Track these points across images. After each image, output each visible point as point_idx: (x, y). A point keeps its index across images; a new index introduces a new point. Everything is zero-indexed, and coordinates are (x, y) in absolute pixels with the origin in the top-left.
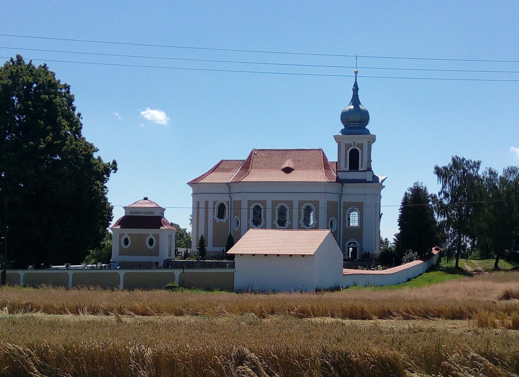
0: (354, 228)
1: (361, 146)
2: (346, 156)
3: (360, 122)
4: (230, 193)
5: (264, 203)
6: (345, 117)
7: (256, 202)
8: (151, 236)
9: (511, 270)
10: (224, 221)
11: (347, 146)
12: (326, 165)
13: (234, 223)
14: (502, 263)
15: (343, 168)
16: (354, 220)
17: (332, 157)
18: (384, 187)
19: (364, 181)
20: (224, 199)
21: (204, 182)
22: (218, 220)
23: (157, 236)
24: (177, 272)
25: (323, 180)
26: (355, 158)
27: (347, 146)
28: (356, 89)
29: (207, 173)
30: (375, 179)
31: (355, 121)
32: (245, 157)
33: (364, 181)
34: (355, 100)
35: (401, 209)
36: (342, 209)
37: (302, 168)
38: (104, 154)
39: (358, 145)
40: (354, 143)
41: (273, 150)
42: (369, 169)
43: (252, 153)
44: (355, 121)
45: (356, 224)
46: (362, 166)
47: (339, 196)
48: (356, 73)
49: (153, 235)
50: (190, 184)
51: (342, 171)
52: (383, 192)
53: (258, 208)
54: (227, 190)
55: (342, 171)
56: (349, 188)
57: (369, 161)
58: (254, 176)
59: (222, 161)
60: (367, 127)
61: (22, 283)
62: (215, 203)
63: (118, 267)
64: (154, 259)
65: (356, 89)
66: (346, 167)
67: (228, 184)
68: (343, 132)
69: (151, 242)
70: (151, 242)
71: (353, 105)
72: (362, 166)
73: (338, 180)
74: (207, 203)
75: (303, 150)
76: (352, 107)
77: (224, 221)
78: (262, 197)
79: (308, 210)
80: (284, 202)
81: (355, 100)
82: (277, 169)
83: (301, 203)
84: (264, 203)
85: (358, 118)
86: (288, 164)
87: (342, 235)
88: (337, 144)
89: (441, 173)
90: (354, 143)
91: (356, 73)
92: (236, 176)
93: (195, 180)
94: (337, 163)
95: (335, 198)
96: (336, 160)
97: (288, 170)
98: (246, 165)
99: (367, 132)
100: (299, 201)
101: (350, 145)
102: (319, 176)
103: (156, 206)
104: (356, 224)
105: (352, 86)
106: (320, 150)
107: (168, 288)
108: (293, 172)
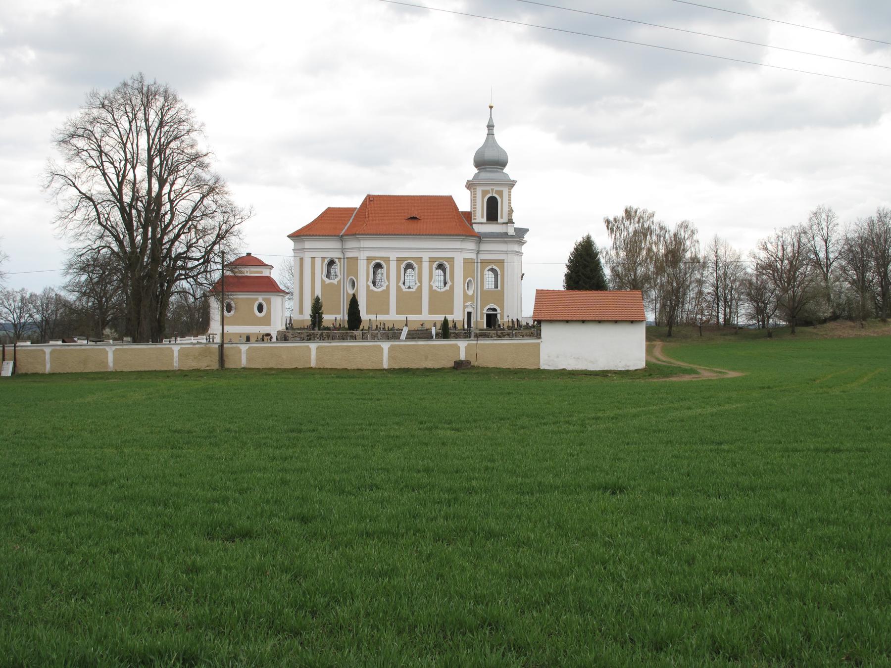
22: (327, 281)
40: (492, 190)
84: (387, 260)
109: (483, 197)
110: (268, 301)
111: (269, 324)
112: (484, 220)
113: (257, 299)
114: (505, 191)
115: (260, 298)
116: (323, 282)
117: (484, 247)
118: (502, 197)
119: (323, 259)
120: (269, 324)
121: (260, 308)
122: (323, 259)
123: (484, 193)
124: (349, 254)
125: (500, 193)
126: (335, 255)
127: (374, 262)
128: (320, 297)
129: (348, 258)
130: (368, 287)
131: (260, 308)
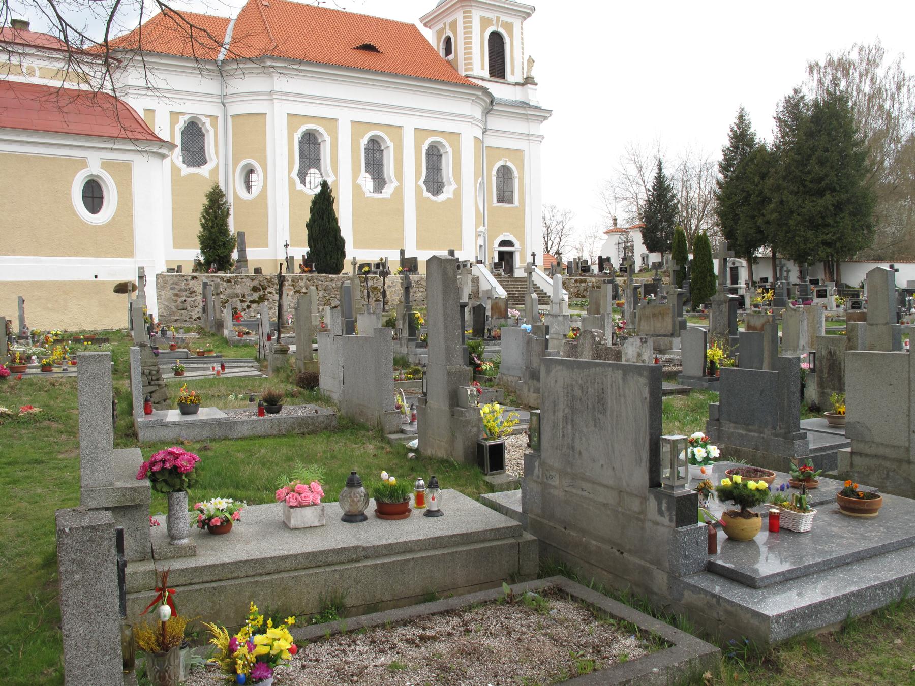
22: (186, 170)
40: (498, 19)
46: (513, 73)
66: (483, 68)
72: (513, 73)
84: (331, 123)
109: (482, 31)
110: (123, 172)
111: (128, 251)
112: (486, 73)
113: (83, 163)
114: (516, 22)
115: (95, 162)
117: (495, 122)
118: (511, 36)
119: (175, 115)
120: (128, 251)
121: (93, 195)
122: (175, 115)
123: (485, 22)
124: (238, 108)
125: (509, 27)
126: (201, 109)
127: (304, 128)
128: (222, 186)
129: (233, 116)
130: (292, 183)
131: (93, 195)
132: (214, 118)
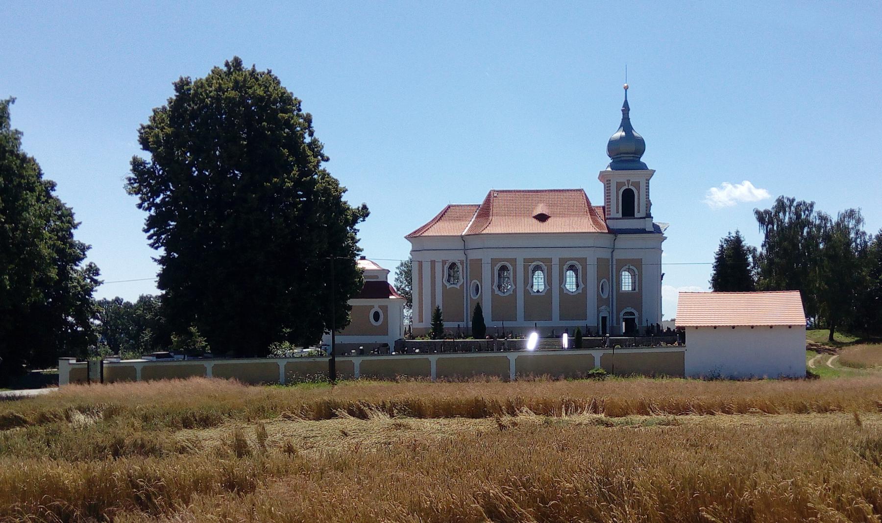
0: (627, 293)
1: (637, 185)
2: (617, 199)
3: (635, 153)
4: (465, 250)
5: (513, 261)
6: (614, 148)
7: (572, 259)
8: (376, 309)
9: (853, 343)
10: (458, 287)
11: (619, 185)
12: (592, 211)
13: (472, 290)
14: (838, 337)
15: (613, 214)
16: (627, 283)
17: (598, 199)
18: (666, 238)
19: (643, 231)
20: (456, 257)
21: (430, 234)
22: (449, 286)
23: (385, 309)
24: (433, 358)
25: (592, 230)
26: (629, 203)
27: (619, 185)
28: (626, 109)
29: (430, 223)
30: (657, 230)
31: (627, 153)
32: (481, 201)
33: (643, 231)
34: (626, 124)
35: (716, 266)
36: (614, 270)
37: (562, 215)
38: (352, 200)
39: (633, 184)
40: (628, 181)
41: (519, 191)
42: (649, 216)
43: (489, 195)
44: (627, 153)
45: (542, 288)
47: (611, 250)
48: (626, 88)
49: (380, 307)
50: (409, 237)
51: (613, 219)
52: (664, 245)
53: (504, 268)
54: (460, 245)
55: (613, 219)
56: (624, 241)
57: (649, 205)
58: (498, 226)
59: (449, 207)
60: (642, 160)
61: (512, 377)
62: (444, 262)
63: (417, 351)
64: (380, 339)
65: (626, 109)
66: (618, 212)
67: (462, 236)
68: (611, 165)
69: (376, 316)
70: (376, 316)
71: (624, 130)
73: (611, 231)
74: (433, 263)
75: (537, 191)
76: (624, 134)
77: (458, 287)
78: (509, 254)
79: (504, 268)
80: (538, 260)
81: (626, 124)
82: (529, 216)
83: (494, 261)
84: (513, 261)
85: (632, 147)
86: (540, 209)
87: (615, 304)
88: (602, 185)
89: (762, 218)
90: (628, 181)
91: (626, 88)
92: (471, 226)
93: (415, 232)
94: (604, 208)
95: (606, 254)
96: (603, 204)
97: (542, 218)
98: (485, 211)
99: (644, 167)
100: (481, 260)
101: (623, 184)
102: (585, 225)
103: (375, 267)
104: (542, 288)
105: (621, 107)
106: (581, 190)
107: (589, 376)
108: (550, 220)
116: (444, 286)
132: (462, 262)
